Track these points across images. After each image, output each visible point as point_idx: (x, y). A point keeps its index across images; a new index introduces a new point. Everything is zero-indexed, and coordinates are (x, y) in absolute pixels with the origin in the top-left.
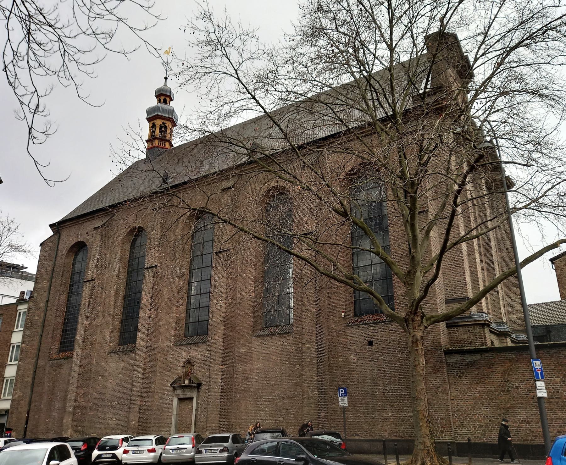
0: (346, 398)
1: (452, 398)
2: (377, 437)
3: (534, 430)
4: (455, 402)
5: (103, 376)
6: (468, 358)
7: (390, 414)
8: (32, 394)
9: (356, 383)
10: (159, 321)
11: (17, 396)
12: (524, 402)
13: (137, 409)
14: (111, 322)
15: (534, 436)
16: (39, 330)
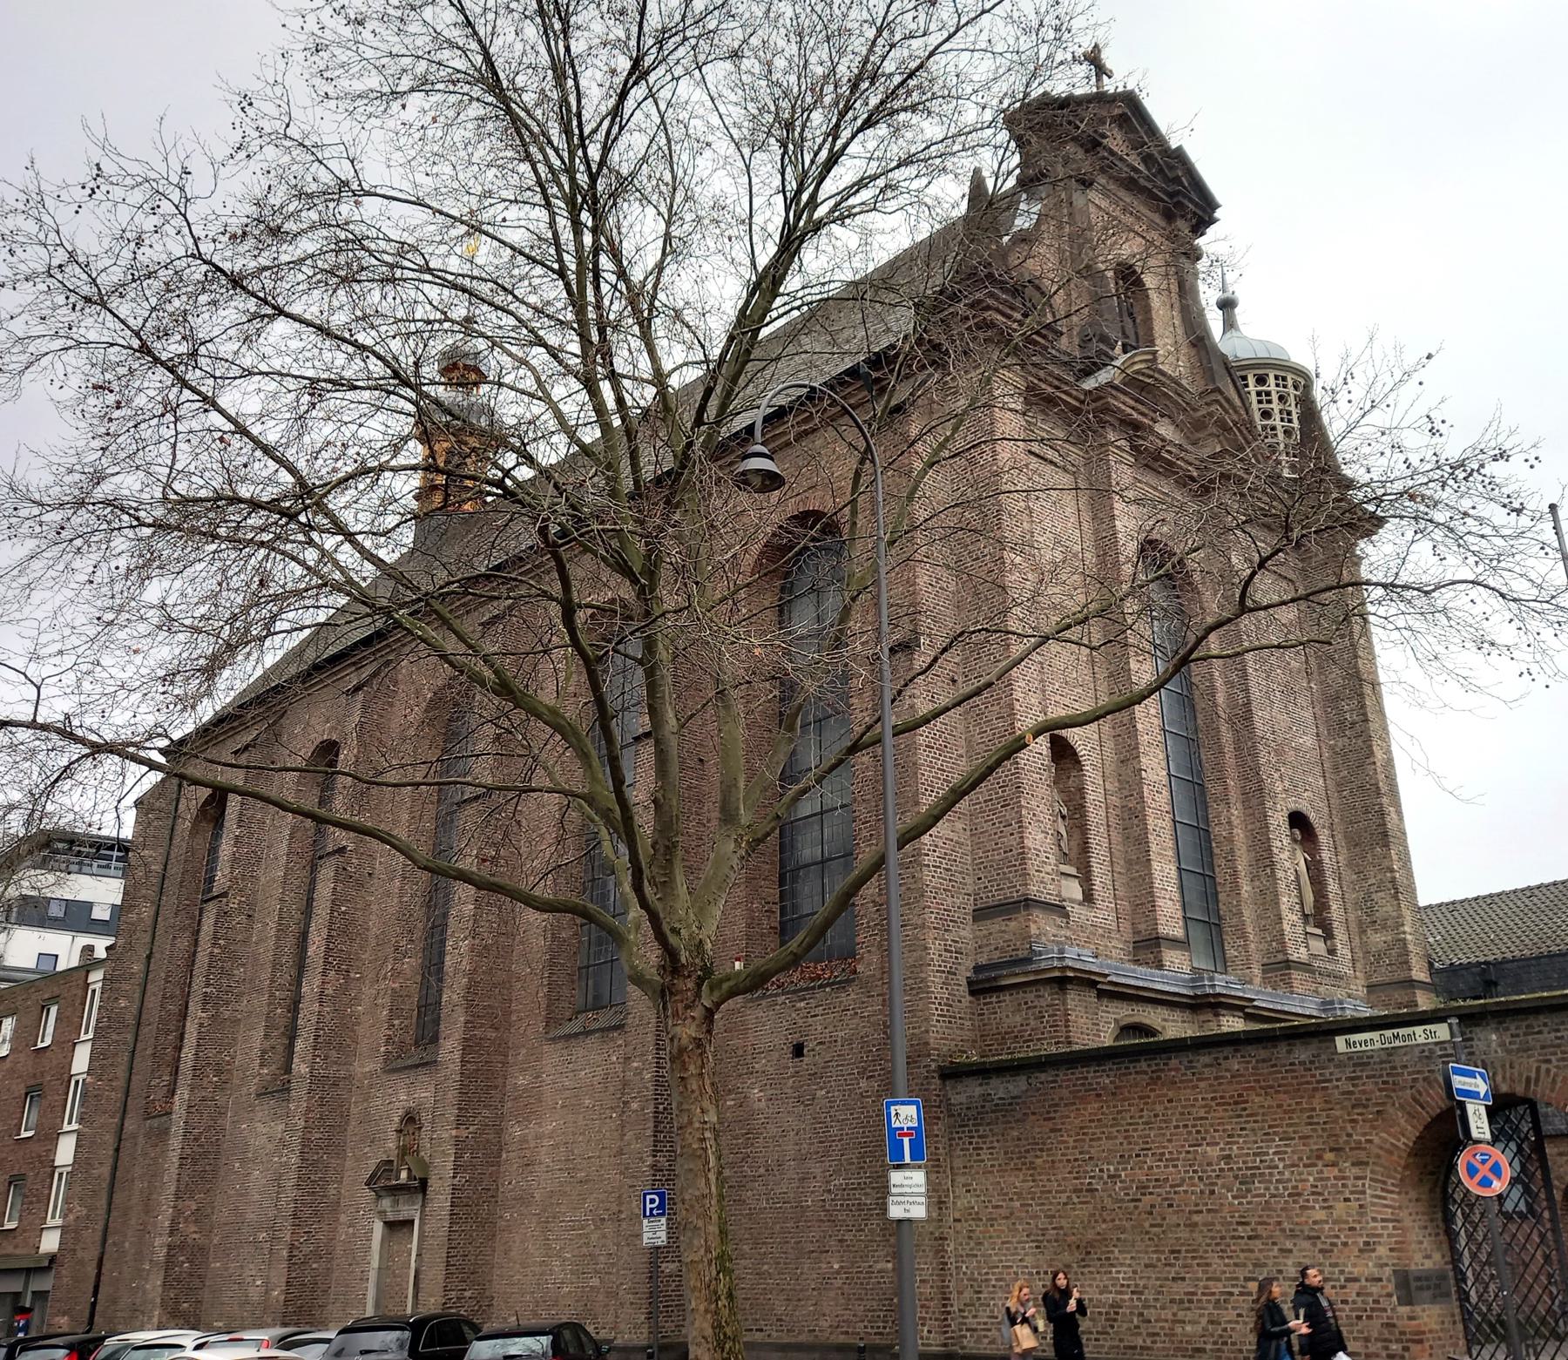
0: (663, 1220)
1: (957, 1216)
2: (803, 1338)
3: (1150, 1314)
4: (963, 1227)
5: (243, 1161)
6: (1000, 1089)
7: (836, 1266)
8: (109, 1211)
9: (762, 1170)
10: (356, 1000)
11: (71, 1217)
12: (1128, 1225)
13: (285, 1253)
14: (265, 1010)
15: (1149, 1335)
16: (130, 1037)
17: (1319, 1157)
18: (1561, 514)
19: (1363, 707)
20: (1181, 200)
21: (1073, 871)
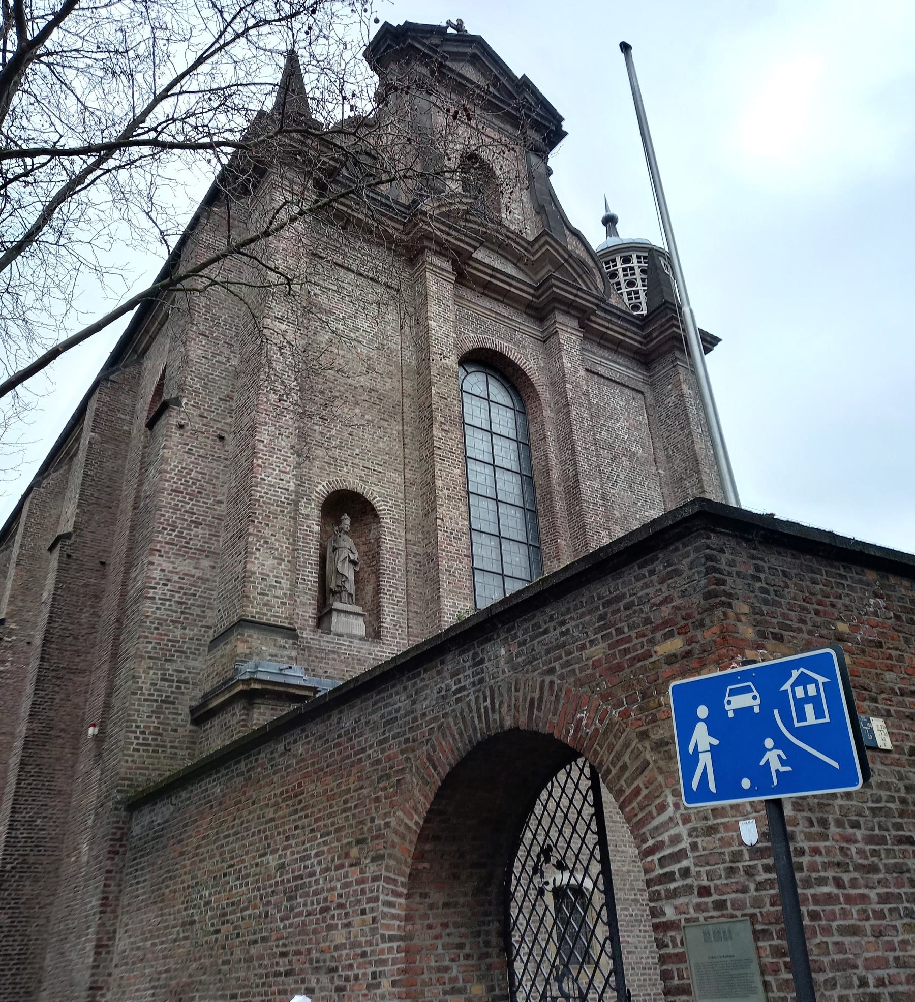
17: (347, 855)
18: (634, 52)
19: (700, 481)
20: (537, 124)
21: (358, 609)
